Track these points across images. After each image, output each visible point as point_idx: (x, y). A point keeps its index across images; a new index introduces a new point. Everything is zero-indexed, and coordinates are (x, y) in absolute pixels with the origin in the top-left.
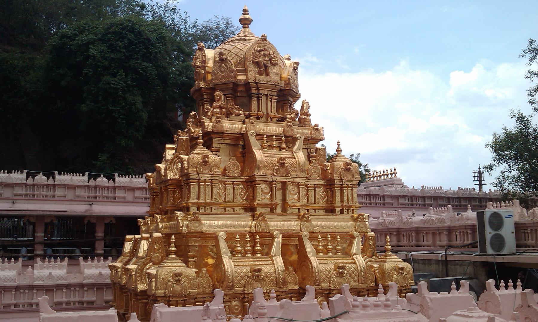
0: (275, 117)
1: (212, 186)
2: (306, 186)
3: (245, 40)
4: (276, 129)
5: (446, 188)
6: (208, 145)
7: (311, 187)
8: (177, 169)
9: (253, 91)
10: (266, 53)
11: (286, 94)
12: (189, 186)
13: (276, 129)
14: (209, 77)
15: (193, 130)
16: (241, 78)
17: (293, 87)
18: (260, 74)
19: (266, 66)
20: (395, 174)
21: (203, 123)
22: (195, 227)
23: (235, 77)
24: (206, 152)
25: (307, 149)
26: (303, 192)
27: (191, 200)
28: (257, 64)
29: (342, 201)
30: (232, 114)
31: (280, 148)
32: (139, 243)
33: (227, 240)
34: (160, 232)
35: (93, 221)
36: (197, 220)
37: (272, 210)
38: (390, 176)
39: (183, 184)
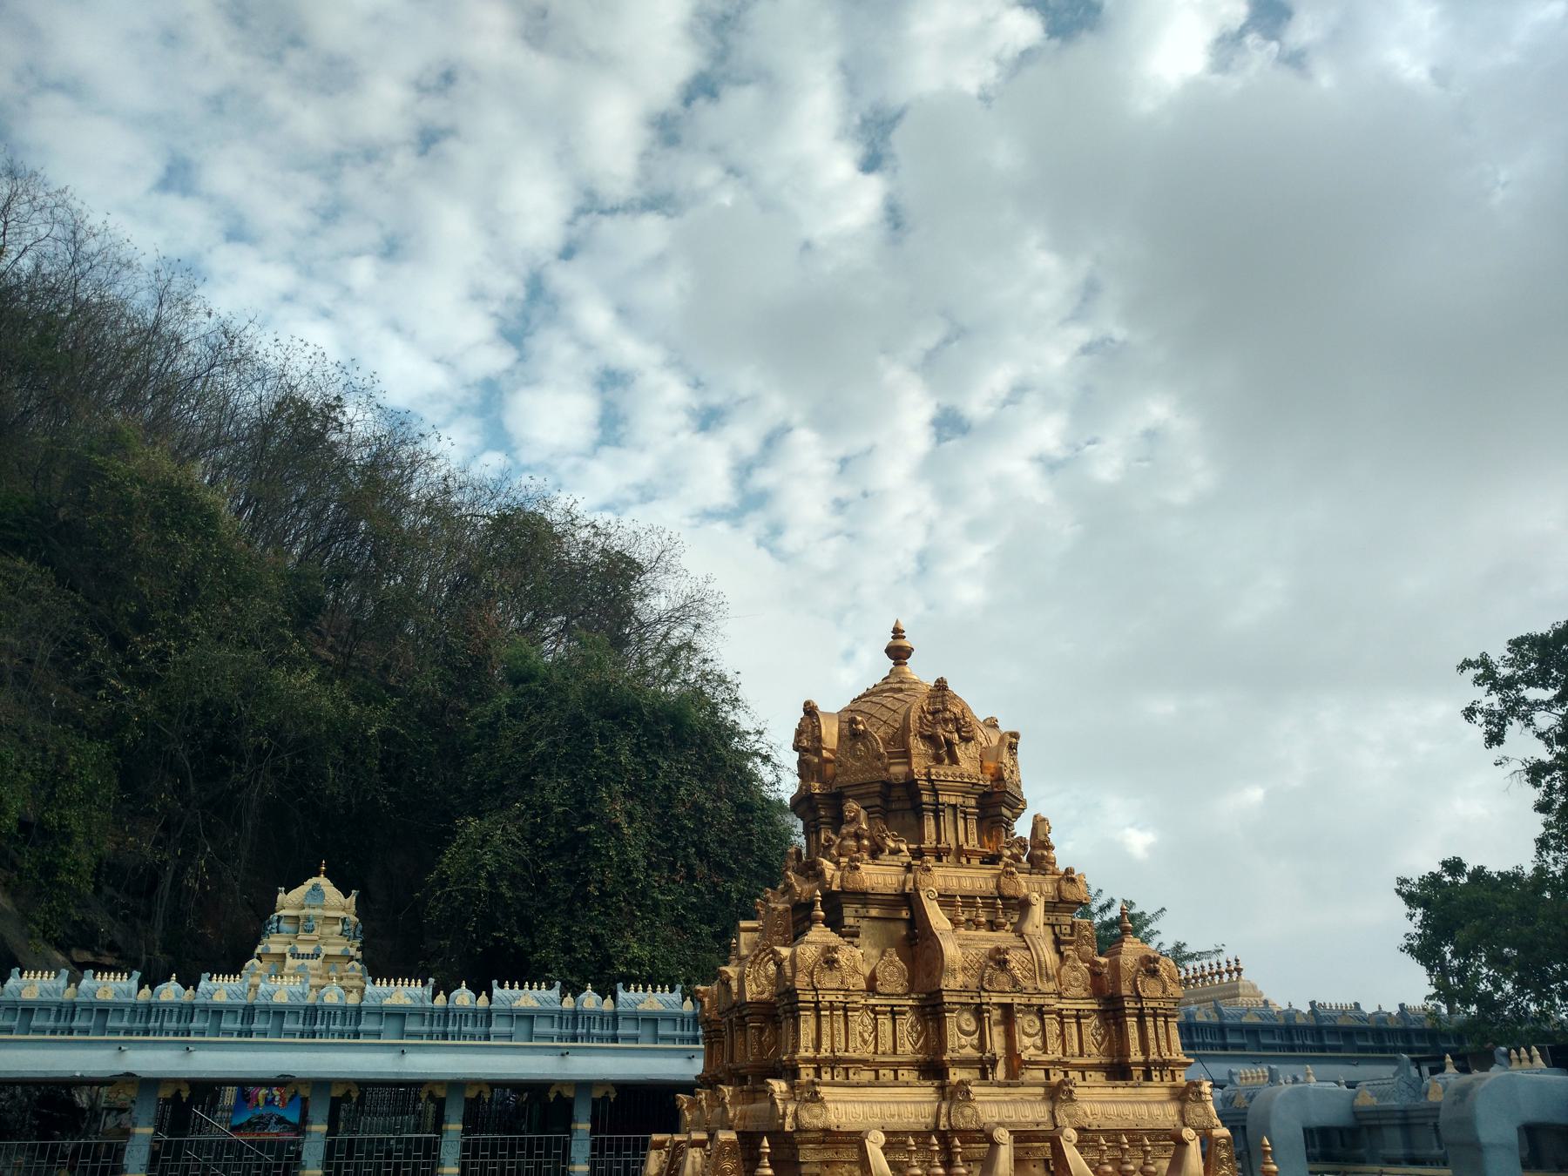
0: (973, 852)
1: (846, 1016)
2: (1059, 1013)
3: (901, 690)
4: (976, 879)
5: (1369, 1008)
6: (834, 923)
7: (1069, 1017)
8: (767, 977)
9: (925, 798)
10: (948, 715)
11: (995, 802)
12: (796, 1019)
13: (976, 879)
14: (830, 769)
15: (798, 889)
16: (898, 770)
17: (1010, 788)
18: (938, 760)
19: (950, 744)
20: (1239, 971)
21: (822, 873)
22: (812, 1118)
23: (886, 770)
24: (833, 939)
25: (1053, 926)
26: (1053, 1027)
27: (802, 1053)
28: (931, 739)
29: (1145, 1049)
30: (882, 851)
31: (993, 926)
32: (683, 1152)
33: (886, 1149)
34: (730, 1128)
35: (568, 1093)
36: (815, 1098)
37: (984, 1076)
38: (1226, 977)
39: (781, 1009)
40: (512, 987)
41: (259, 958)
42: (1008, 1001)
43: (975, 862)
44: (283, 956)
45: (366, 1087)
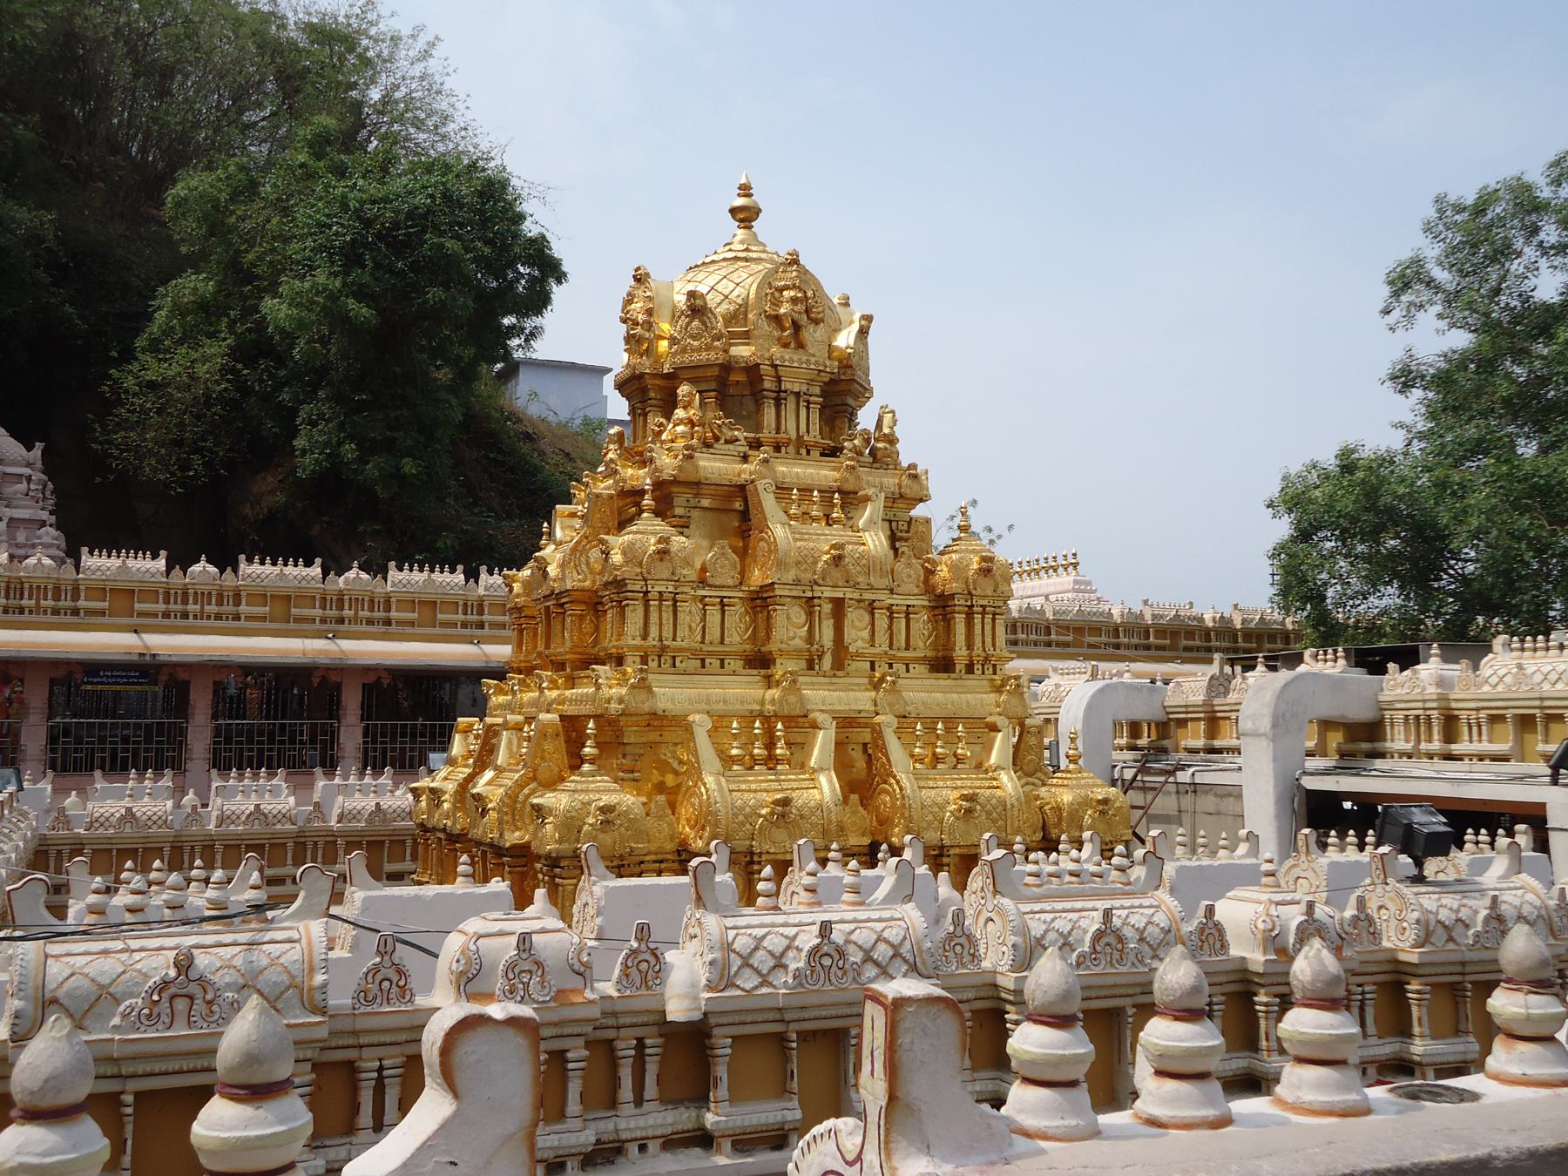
43: (815, 454)
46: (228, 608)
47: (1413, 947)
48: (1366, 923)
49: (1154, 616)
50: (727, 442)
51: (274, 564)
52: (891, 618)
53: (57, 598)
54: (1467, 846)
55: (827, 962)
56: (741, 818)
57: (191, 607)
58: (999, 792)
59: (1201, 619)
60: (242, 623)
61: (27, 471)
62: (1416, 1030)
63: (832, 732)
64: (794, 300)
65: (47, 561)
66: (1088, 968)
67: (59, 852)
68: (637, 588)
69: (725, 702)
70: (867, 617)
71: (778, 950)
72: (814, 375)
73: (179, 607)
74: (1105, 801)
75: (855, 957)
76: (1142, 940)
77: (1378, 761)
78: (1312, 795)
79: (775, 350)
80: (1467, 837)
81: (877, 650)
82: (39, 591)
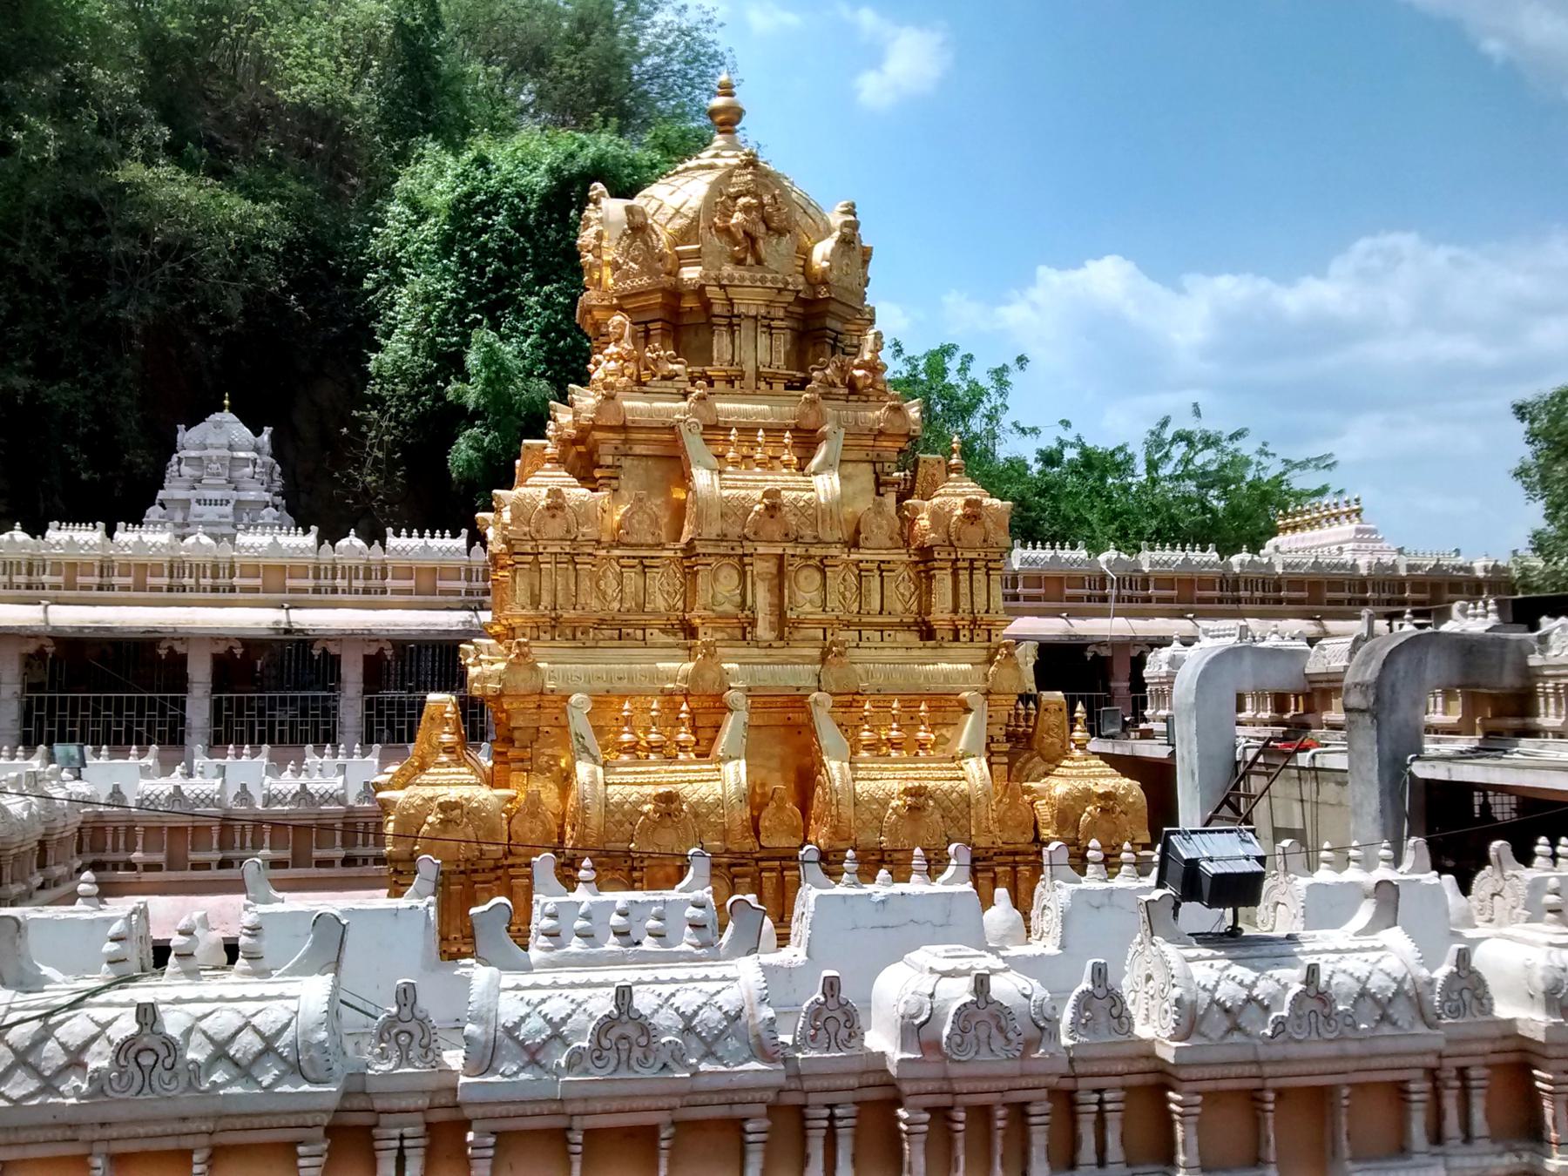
35: (1105, 652)
40: (410, 536)
41: (162, 505)
42: (780, 551)
43: (779, 387)
44: (189, 501)
45: (253, 645)
46: (375, 583)
47: (1171, 1038)
48: (1106, 1003)
49: (1410, 567)
50: (664, 378)
51: (421, 536)
52: (955, 574)
53: (215, 576)
54: (1538, 860)
55: (147, 1060)
56: (618, 817)
57: (339, 582)
58: (963, 785)
59: (1470, 569)
60: (388, 597)
61: (252, 455)
62: (1181, 1158)
63: (744, 716)
64: (746, 209)
65: (206, 540)
66: (586, 1072)
67: (116, 829)
68: (944, 555)
69: (631, 679)
70: (817, 576)
71: (74, 1041)
72: (773, 295)
73: (345, 583)
74: (1107, 796)
75: (196, 1053)
76: (688, 1029)
77: (1523, 741)
78: (1433, 788)
79: (728, 269)
80: (1538, 849)
81: (831, 615)
82: (197, 570)
